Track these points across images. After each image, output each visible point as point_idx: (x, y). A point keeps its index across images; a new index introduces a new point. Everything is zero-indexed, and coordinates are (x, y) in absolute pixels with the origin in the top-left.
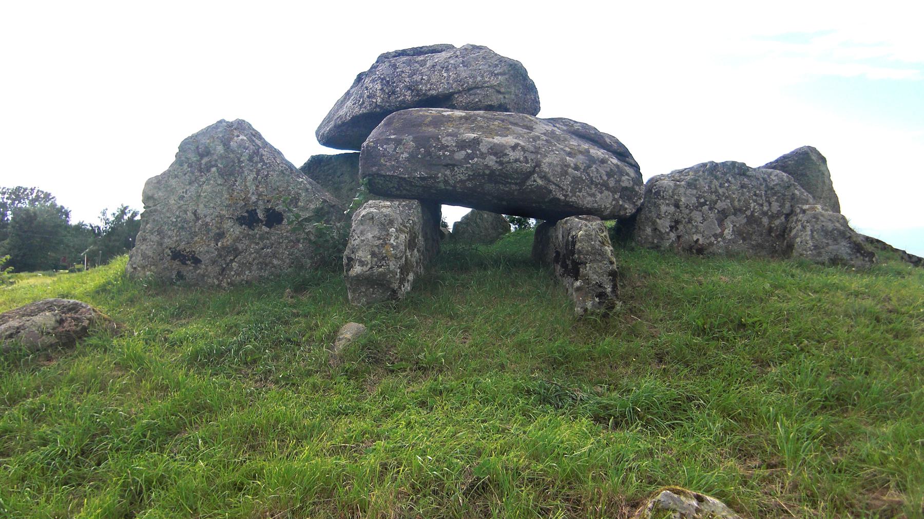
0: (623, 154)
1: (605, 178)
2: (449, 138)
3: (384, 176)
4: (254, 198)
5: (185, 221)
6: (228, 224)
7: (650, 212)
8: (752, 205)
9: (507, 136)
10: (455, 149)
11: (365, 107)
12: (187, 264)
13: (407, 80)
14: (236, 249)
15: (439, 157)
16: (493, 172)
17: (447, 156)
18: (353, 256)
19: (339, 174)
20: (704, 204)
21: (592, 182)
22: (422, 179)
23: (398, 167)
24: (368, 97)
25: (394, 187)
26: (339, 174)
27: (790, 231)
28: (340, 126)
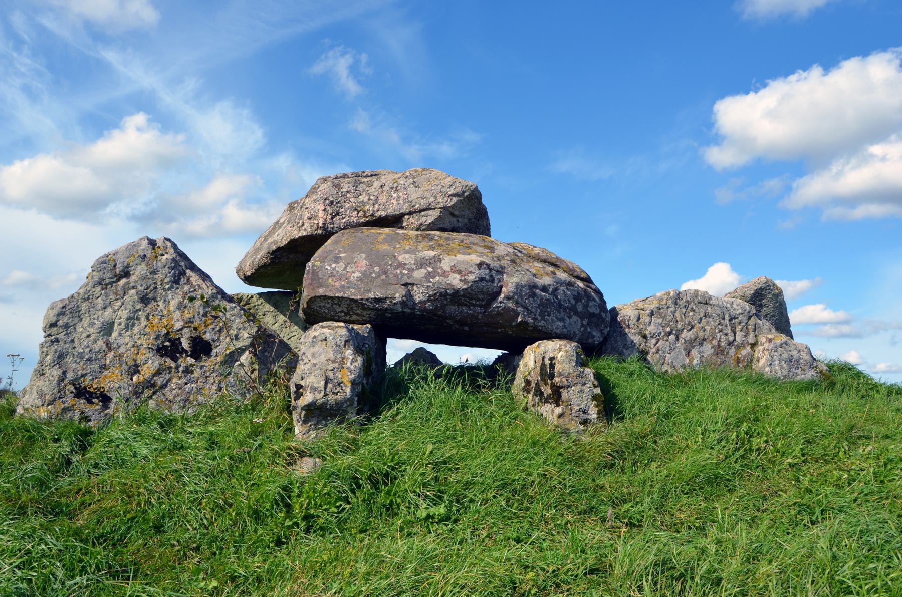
0: (588, 280)
1: (573, 302)
2: (407, 256)
3: (332, 298)
4: (178, 325)
7: (616, 341)
8: (718, 335)
9: (469, 254)
10: (414, 267)
11: (305, 230)
12: (93, 403)
13: (352, 200)
14: (153, 385)
15: (396, 276)
16: (456, 292)
17: (404, 274)
18: (302, 383)
20: (670, 333)
21: (560, 305)
23: (349, 288)
24: (309, 218)
25: (342, 311)
27: (758, 361)
28: (274, 252)
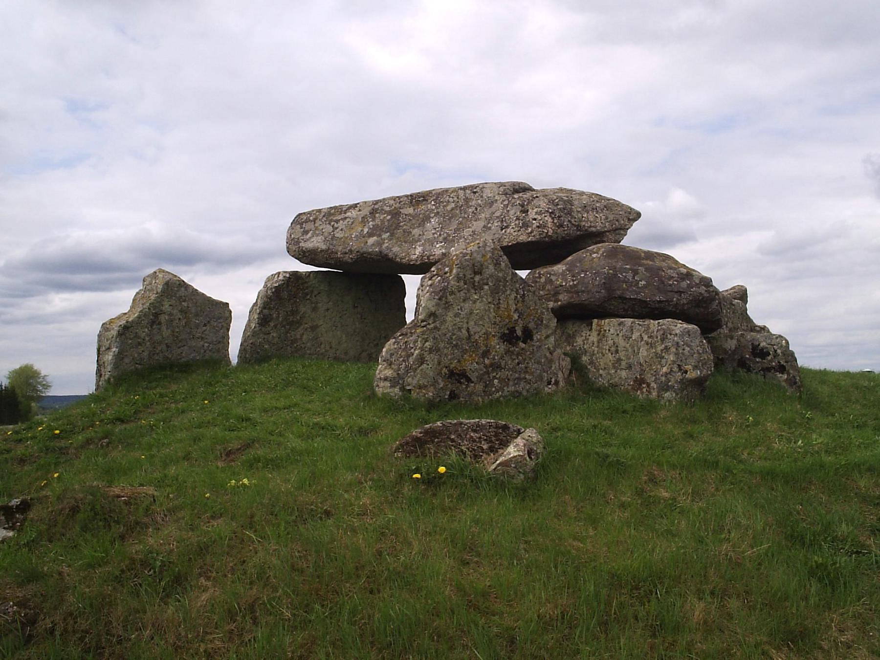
5: (460, 339)
6: (494, 342)
19: (316, 292)
22: (660, 302)
26: (316, 292)
